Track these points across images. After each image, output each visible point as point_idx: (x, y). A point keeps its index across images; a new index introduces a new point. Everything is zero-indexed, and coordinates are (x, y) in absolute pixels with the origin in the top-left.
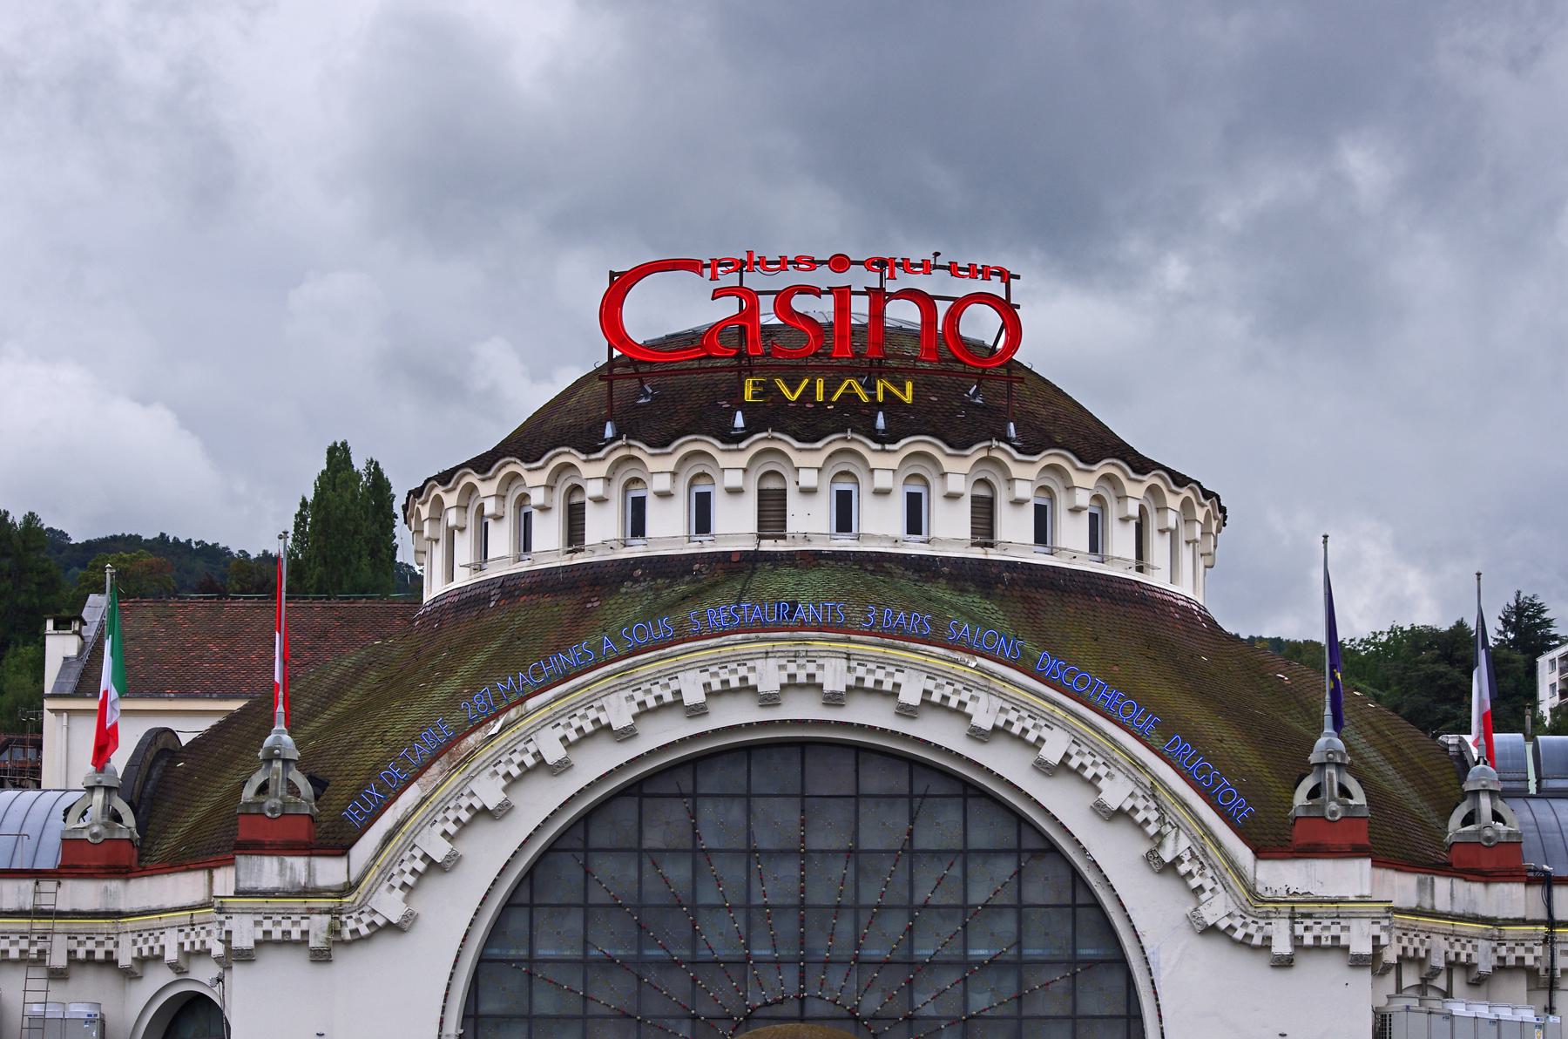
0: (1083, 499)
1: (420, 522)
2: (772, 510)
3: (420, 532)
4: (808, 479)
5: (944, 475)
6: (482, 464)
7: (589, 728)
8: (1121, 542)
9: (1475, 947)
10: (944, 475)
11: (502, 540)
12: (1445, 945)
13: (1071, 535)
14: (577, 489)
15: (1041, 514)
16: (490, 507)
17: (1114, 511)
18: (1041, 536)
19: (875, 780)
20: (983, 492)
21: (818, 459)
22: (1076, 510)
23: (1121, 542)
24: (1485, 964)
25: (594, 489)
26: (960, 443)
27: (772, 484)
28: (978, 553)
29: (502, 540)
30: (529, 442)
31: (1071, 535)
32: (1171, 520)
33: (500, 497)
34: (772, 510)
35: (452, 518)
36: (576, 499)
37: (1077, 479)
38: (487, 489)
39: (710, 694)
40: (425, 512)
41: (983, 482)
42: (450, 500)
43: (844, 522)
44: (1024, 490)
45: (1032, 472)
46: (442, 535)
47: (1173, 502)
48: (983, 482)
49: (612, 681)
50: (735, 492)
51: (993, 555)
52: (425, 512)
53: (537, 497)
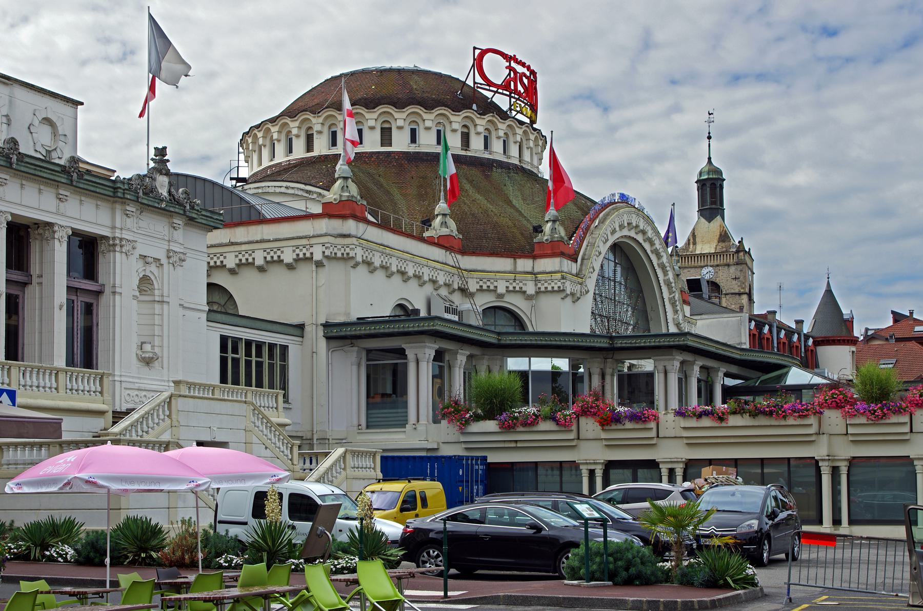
0: (501, 133)
1: (248, 145)
2: (386, 136)
3: (248, 148)
4: (400, 123)
5: (451, 122)
6: (273, 121)
7: (517, 289)
8: (514, 151)
9: (225, 258)
10: (451, 122)
11: (280, 149)
12: (428, 271)
13: (497, 147)
14: (310, 128)
15: (486, 139)
16: (275, 136)
17: (511, 139)
18: (486, 147)
19: (881, 542)
20: (466, 130)
21: (404, 115)
22: (499, 138)
23: (514, 151)
24: (377, 263)
25: (317, 127)
26: (456, 109)
27: (386, 125)
28: (463, 153)
29: (280, 149)
30: (291, 112)
31: (497, 147)
32: (531, 144)
33: (279, 132)
34: (386, 136)
35: (261, 141)
36: (310, 132)
37: (500, 126)
38: (274, 129)
39: (508, 291)
40: (250, 140)
41: (465, 126)
42: (260, 135)
43: (413, 139)
44: (480, 129)
45: (483, 122)
46: (257, 148)
47: (532, 137)
48: (465, 126)
49: (300, 193)
50: (372, 128)
51: (469, 154)
52: (250, 140)
53: (295, 131)
